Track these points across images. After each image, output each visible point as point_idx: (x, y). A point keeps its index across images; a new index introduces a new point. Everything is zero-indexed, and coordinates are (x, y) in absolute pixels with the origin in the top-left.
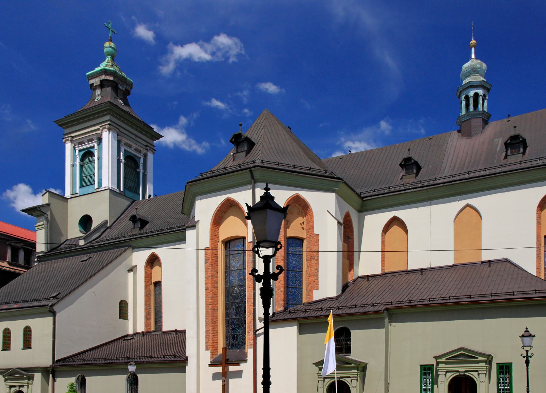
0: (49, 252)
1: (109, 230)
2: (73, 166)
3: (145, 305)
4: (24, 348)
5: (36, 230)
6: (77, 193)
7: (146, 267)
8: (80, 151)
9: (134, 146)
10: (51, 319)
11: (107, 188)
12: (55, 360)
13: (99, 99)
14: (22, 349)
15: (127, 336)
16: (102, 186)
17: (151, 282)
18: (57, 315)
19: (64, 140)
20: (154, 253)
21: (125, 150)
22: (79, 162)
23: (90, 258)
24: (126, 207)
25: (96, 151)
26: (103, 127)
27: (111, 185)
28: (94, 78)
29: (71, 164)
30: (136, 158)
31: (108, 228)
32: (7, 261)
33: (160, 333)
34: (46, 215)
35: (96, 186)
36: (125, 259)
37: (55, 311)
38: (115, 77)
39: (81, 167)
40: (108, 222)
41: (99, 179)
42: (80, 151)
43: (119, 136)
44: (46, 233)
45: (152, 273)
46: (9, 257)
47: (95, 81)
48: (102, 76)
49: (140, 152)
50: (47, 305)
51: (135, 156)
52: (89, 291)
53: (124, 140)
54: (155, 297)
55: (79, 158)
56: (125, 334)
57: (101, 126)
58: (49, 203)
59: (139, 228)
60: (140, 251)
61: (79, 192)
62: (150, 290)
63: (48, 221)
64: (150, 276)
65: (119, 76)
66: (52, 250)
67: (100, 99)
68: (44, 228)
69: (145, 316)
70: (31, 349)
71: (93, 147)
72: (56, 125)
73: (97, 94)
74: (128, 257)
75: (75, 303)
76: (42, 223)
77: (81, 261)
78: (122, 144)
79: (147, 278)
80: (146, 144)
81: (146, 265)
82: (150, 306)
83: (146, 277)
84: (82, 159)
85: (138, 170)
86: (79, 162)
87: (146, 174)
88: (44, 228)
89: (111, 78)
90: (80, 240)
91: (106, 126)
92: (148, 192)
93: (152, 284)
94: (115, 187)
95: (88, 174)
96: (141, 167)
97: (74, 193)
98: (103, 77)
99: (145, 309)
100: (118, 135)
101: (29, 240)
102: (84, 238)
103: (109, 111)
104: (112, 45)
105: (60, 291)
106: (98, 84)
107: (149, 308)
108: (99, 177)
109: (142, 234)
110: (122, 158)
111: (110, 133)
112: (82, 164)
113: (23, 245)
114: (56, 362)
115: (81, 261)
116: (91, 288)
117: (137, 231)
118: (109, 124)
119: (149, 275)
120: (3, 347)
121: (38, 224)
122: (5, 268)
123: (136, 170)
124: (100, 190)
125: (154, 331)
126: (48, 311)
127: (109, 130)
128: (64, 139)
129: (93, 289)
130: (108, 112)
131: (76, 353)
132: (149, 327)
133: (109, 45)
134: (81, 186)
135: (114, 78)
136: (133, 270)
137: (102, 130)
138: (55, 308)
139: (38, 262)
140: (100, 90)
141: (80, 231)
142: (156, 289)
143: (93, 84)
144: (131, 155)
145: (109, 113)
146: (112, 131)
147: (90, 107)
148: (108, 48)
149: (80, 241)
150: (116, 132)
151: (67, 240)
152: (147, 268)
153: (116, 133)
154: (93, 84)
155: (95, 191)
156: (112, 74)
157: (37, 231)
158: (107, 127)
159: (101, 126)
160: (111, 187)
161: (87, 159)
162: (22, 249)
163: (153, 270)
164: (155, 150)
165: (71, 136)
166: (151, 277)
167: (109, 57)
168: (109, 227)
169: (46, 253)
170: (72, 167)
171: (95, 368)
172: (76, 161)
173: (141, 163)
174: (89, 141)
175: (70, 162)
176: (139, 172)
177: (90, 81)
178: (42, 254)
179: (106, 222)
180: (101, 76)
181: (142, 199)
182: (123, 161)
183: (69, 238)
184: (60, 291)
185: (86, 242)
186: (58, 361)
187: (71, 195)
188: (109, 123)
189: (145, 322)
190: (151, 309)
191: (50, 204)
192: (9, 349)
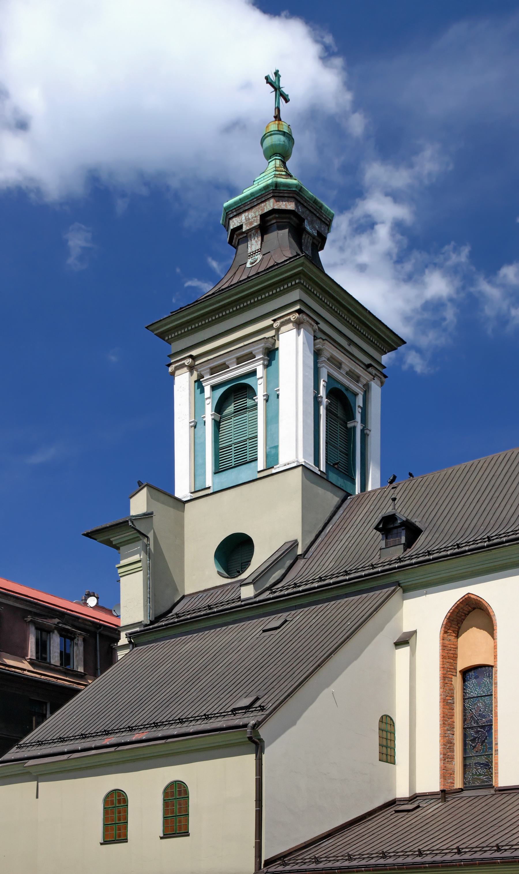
0: (152, 623)
1: (301, 562)
2: (195, 427)
3: (441, 725)
4: (164, 835)
5: (120, 575)
6: (209, 488)
7: (445, 632)
8: (214, 388)
9: (348, 364)
10: (251, 758)
11: (295, 465)
12: (264, 859)
13: (258, 261)
14: (161, 838)
15: (393, 802)
16: (277, 463)
17: (455, 669)
18: (267, 750)
19: (171, 369)
20: (472, 596)
21: (329, 376)
22: (212, 415)
23: (286, 621)
24: (332, 509)
25: (260, 381)
26: (282, 320)
27: (304, 458)
28: (245, 211)
29: (190, 423)
30: (348, 395)
31: (297, 558)
32: (29, 657)
33: (492, 791)
34: (145, 540)
35: (261, 464)
36: (388, 620)
37: (261, 740)
38: (298, 203)
39: (217, 425)
40: (298, 545)
41: (267, 448)
42: (214, 388)
43: (318, 341)
44: (146, 580)
45: (457, 648)
46: (31, 649)
47: (247, 219)
48: (267, 202)
49: (357, 379)
50: (245, 726)
51: (347, 389)
52: (326, 694)
53: (329, 350)
54: (464, 706)
55: (212, 404)
56: (390, 798)
57: (274, 320)
58: (149, 511)
59: (404, 544)
60: (426, 594)
61: (213, 483)
62: (452, 690)
63: (148, 552)
64: (452, 655)
65: (306, 201)
66: (157, 619)
67: (261, 260)
68: (141, 569)
69: (441, 754)
70: (188, 835)
71: (253, 373)
72: (151, 336)
73: (249, 251)
74: (395, 615)
75: (300, 722)
76: (136, 557)
77: (264, 631)
78: (323, 359)
79: (447, 660)
80: (368, 361)
81: (445, 627)
82: (452, 727)
83: (443, 657)
84: (219, 408)
85: (350, 425)
86: (212, 415)
87: (368, 432)
88: (141, 569)
89: (290, 206)
90: (241, 586)
91: (291, 316)
92: (372, 472)
93: (459, 675)
94: (311, 463)
95: (250, 436)
96: (358, 417)
97: (197, 490)
98: (270, 205)
99: (441, 734)
100: (315, 338)
101: (68, 612)
102: (253, 580)
103: (300, 279)
104: (284, 127)
105: (258, 694)
106: (256, 223)
107: (451, 732)
108: (268, 443)
109: (411, 558)
110: (322, 392)
111: (299, 334)
112: (218, 419)
113: (59, 623)
114: (265, 866)
115: (264, 631)
116: (328, 685)
117: (397, 552)
118: (299, 311)
119: (452, 652)
120: (105, 835)
121: (123, 562)
122: (26, 672)
123: (346, 423)
124: (274, 471)
125: (462, 790)
126: (247, 739)
127: (298, 324)
128: (169, 365)
129: (332, 688)
130: (297, 281)
131: (303, 842)
132: (451, 780)
133: (277, 129)
134: (217, 471)
135: (296, 205)
136: (410, 641)
137: (278, 330)
138: (263, 732)
139: (131, 646)
140: (260, 238)
141: (219, 573)
142: (467, 686)
143: (241, 227)
144: (339, 386)
145: (299, 283)
146: (305, 329)
147: (235, 281)
148: (273, 136)
149: (243, 589)
150: (310, 329)
151: (183, 597)
152: (446, 635)
153: (313, 332)
154: (241, 227)
155: (258, 477)
156: (291, 195)
157: (121, 579)
158: (292, 319)
159: (274, 320)
160: (305, 462)
161: (233, 405)
162: (56, 632)
163: (460, 639)
164: (386, 377)
165: (191, 356)
166: (455, 657)
167: (276, 159)
168: (301, 555)
169: (146, 625)
170: (193, 428)
171: (415, 871)
172: (204, 413)
173: (359, 406)
174: (240, 360)
175: (188, 417)
176: (354, 428)
177: (231, 221)
178: (138, 629)
179: (295, 544)
180: (263, 205)
181: (378, 486)
182: (325, 400)
183: (187, 593)
184: (260, 694)
185: (258, 591)
186: (268, 863)
187: (191, 493)
188: (297, 307)
189: (441, 767)
190: (455, 736)
191: (152, 513)
192: (125, 840)
